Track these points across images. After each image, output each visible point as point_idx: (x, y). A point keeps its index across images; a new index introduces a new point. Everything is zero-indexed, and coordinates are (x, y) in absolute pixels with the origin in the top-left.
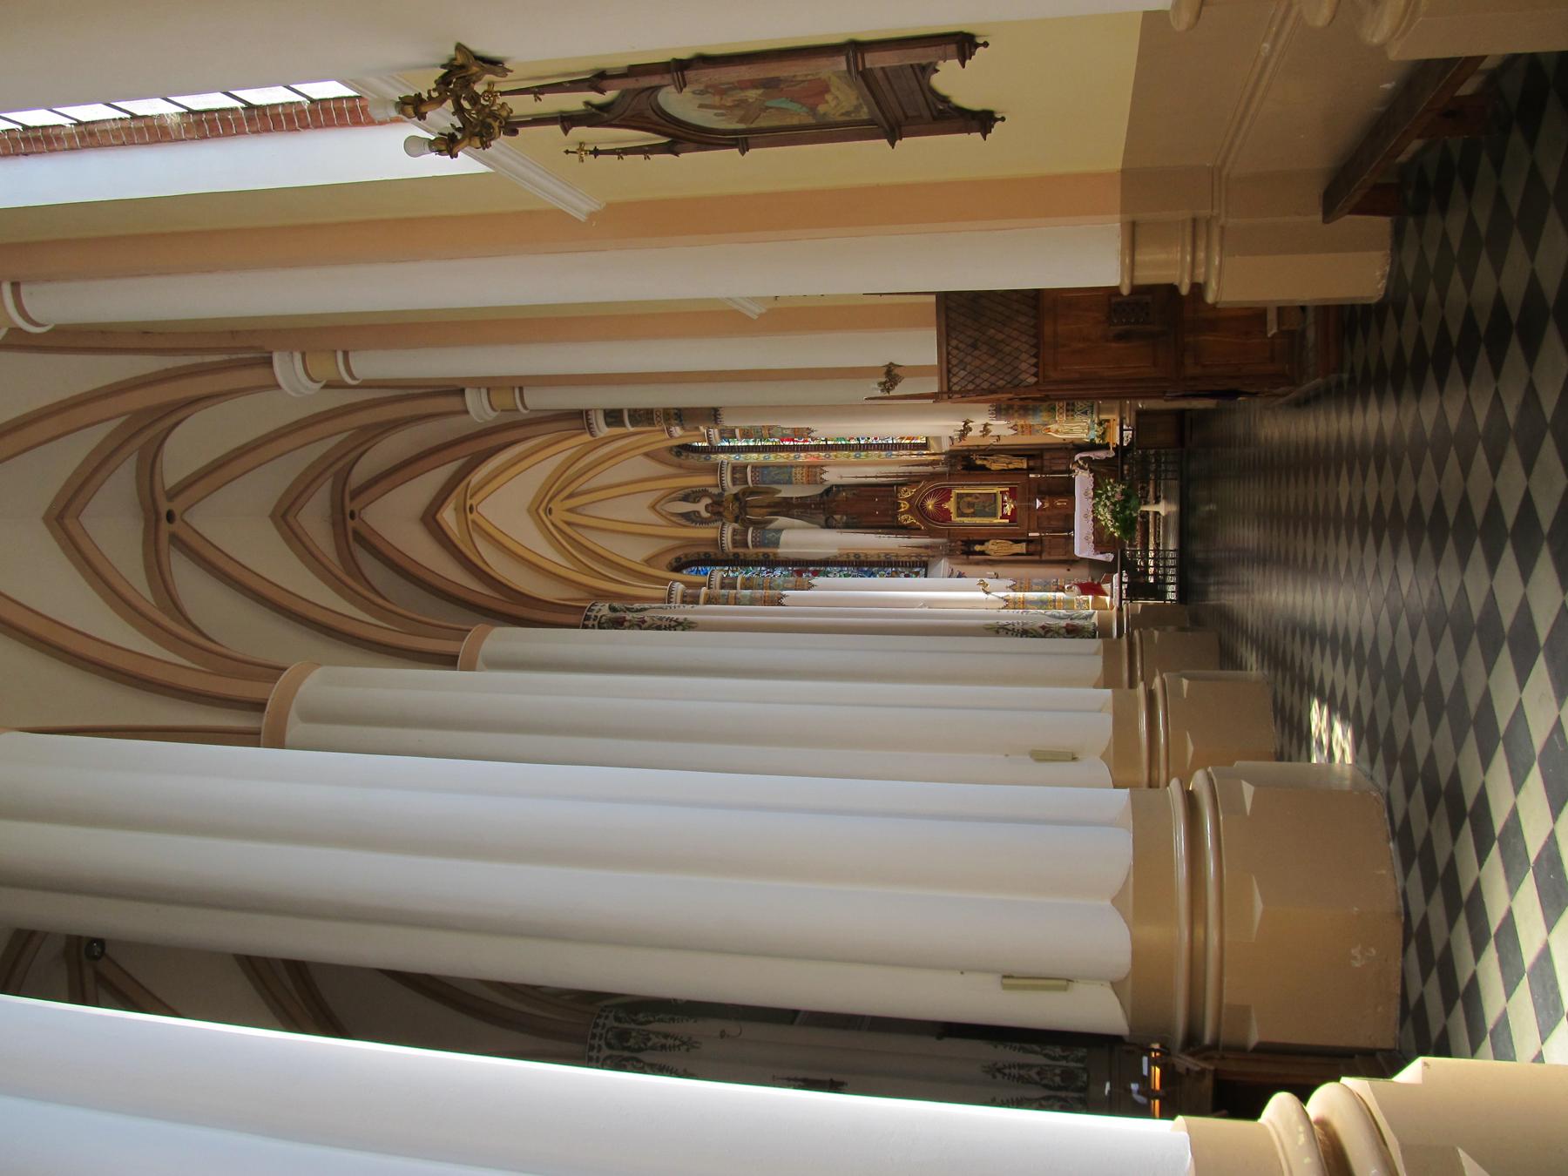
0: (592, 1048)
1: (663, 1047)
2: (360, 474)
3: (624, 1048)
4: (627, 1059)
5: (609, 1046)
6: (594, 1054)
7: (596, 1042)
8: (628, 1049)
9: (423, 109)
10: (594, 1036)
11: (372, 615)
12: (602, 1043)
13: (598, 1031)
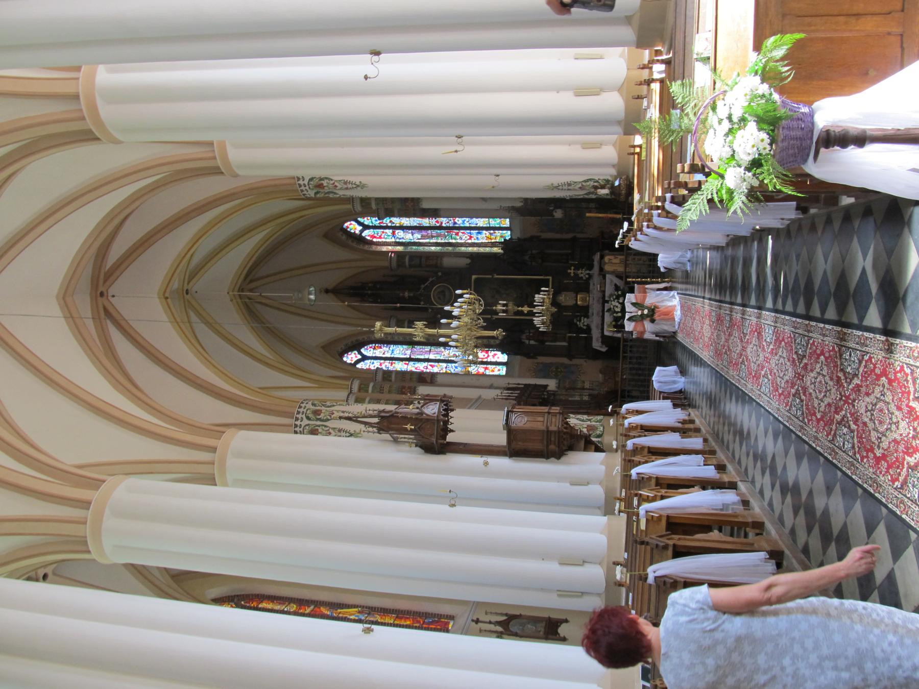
0: (297, 419)
5: (308, 418)
7: (299, 416)
10: (298, 413)
11: (166, 422)
12: (304, 416)
13: (301, 410)
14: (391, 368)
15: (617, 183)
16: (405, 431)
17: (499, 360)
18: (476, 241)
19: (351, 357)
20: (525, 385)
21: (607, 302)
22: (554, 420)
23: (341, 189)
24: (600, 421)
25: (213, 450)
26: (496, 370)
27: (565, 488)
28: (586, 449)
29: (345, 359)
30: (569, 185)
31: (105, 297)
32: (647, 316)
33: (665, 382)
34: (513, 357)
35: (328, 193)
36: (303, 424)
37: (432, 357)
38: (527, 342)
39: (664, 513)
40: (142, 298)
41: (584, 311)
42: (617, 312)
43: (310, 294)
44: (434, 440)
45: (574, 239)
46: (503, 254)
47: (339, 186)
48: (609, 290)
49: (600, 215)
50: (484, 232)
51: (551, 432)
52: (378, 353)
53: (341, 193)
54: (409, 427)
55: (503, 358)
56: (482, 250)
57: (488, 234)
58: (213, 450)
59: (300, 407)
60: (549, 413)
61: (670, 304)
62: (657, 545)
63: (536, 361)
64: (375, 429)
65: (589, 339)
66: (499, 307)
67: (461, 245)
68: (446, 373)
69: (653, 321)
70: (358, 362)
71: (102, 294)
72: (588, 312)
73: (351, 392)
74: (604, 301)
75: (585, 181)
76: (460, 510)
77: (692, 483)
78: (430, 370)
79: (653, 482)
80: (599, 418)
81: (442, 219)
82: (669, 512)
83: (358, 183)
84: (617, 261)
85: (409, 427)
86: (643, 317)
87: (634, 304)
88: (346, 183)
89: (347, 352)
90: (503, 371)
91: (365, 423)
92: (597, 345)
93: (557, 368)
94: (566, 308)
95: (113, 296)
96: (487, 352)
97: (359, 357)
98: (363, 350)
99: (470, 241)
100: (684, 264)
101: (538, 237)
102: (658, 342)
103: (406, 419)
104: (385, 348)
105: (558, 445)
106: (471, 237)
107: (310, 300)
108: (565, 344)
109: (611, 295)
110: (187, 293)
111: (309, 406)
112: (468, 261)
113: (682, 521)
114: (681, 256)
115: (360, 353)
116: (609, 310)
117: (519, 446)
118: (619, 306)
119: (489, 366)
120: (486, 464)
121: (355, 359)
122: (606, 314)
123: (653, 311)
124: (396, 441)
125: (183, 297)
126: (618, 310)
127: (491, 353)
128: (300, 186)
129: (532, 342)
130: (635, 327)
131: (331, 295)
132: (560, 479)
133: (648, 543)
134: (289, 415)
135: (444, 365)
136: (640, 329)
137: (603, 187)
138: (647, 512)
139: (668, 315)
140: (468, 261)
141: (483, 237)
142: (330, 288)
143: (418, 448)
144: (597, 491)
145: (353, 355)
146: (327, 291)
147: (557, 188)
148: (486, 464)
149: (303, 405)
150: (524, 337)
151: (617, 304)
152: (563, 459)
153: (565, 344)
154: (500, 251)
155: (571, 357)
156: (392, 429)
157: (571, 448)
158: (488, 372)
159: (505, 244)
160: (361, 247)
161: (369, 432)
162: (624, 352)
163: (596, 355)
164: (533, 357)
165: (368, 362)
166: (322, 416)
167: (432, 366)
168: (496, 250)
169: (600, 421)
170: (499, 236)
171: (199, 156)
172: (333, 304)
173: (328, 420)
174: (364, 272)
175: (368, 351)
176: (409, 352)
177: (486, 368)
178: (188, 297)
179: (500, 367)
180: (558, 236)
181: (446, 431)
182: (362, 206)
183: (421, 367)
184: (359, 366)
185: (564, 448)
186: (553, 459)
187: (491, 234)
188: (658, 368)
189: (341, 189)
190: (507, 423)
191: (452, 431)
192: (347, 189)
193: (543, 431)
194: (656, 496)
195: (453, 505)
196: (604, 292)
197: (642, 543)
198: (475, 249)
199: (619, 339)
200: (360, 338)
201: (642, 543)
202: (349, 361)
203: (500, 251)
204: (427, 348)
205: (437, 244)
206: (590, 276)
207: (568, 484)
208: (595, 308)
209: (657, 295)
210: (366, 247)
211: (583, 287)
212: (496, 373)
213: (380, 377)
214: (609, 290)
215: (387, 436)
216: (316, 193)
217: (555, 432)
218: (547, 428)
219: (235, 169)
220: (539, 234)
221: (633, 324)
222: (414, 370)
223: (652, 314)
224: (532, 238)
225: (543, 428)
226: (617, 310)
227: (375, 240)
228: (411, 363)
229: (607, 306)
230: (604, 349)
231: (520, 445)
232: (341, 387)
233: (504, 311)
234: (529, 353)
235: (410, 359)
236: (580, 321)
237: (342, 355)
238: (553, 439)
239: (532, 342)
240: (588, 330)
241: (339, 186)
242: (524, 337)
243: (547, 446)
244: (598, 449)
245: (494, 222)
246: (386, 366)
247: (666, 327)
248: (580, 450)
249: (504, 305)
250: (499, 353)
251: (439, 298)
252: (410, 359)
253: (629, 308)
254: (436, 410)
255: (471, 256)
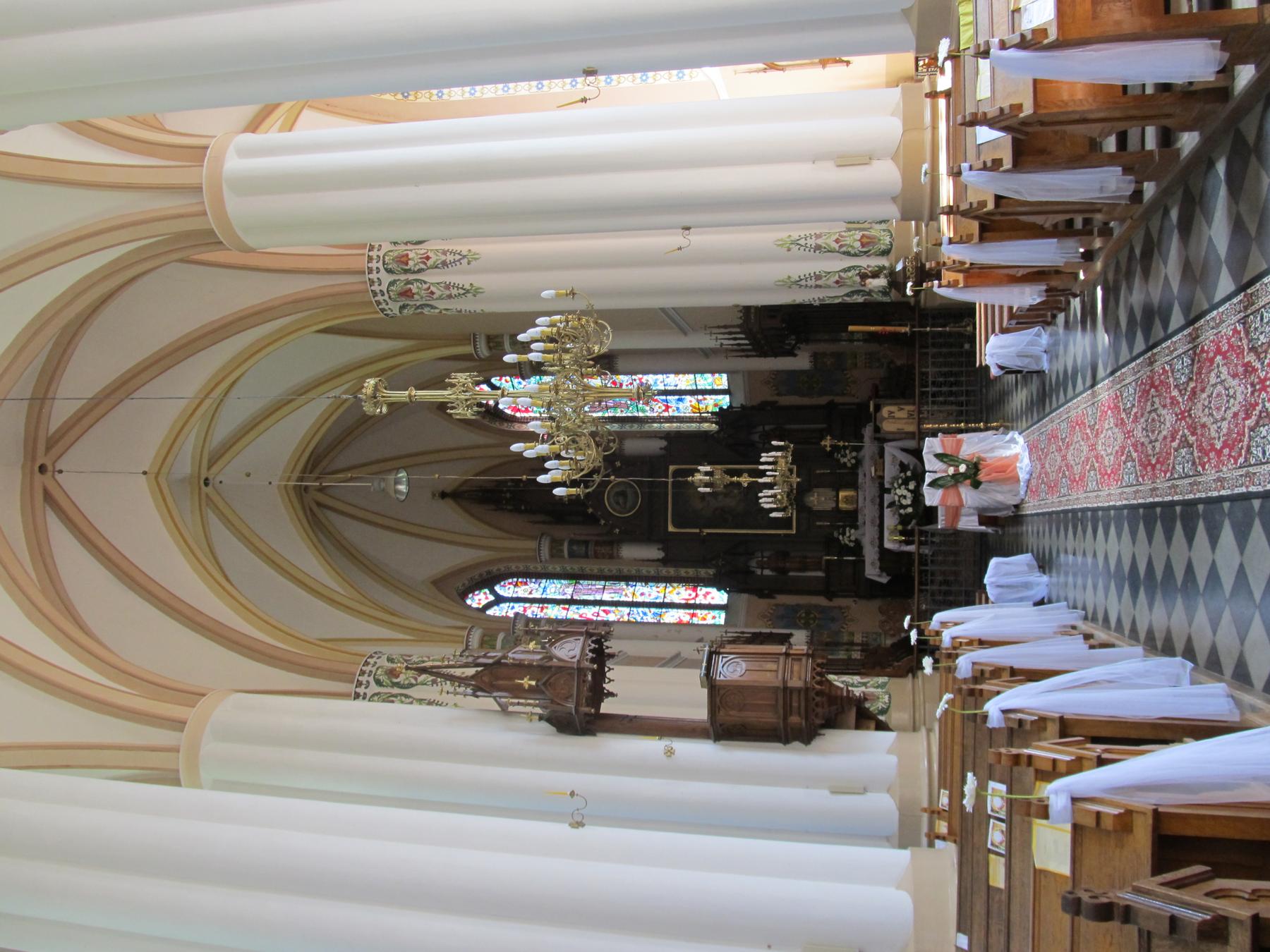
0: (359, 684)
1: (444, 264)
2: (61, 412)
3: (406, 271)
4: (395, 696)
5: (379, 683)
6: (361, 690)
7: (364, 679)
8: (398, 685)
9: (876, 537)
10: (362, 673)
11: (109, 678)
12: (371, 679)
13: (367, 669)
14: (541, 615)
15: (899, 267)
16: (518, 692)
17: (713, 602)
18: (676, 414)
19: (479, 599)
20: (754, 634)
21: (888, 491)
22: (796, 668)
23: (440, 298)
24: (882, 686)
25: (179, 725)
26: (709, 617)
27: (820, 798)
28: (858, 726)
29: (469, 602)
30: (818, 277)
31: (49, 474)
32: (965, 476)
33: (1008, 586)
34: (736, 596)
35: (422, 306)
36: (369, 692)
37: (607, 597)
38: (759, 572)
39: (1145, 802)
40: (117, 487)
41: (851, 518)
42: (905, 507)
43: (397, 482)
44: (571, 705)
45: (831, 404)
46: (718, 432)
47: (438, 293)
48: (890, 471)
49: (872, 328)
50: (688, 398)
51: (792, 690)
52: (522, 592)
53: (442, 305)
54: (527, 682)
55: (720, 597)
56: (685, 427)
57: (694, 403)
58: (179, 725)
59: (366, 663)
60: (787, 655)
61: (1008, 453)
62: (1174, 923)
63: (772, 601)
64: (469, 691)
65: (860, 563)
66: (698, 477)
67: (653, 420)
68: (629, 622)
69: (976, 485)
70: (489, 606)
71: (42, 469)
72: (856, 519)
73: (467, 648)
74: (883, 491)
75: (845, 270)
76: (591, 833)
77: (1167, 736)
78: (603, 617)
79: (1053, 728)
80: (881, 680)
81: (622, 377)
82: (1169, 801)
83: (467, 287)
84: (903, 414)
85: (527, 682)
86: (957, 478)
87: (938, 456)
88: (448, 287)
89: (473, 592)
90: (720, 618)
91: (452, 678)
92: (872, 571)
93: (808, 613)
94: (821, 515)
95: (61, 472)
96: (695, 590)
97: (492, 598)
98: (497, 588)
99: (666, 414)
100: (1037, 359)
101: (773, 404)
102: (983, 535)
103: (522, 668)
104: (532, 585)
105: (805, 715)
106: (667, 408)
107: (397, 491)
108: (820, 574)
109: (895, 479)
110: (206, 484)
111: (383, 662)
112: (663, 443)
113: (1208, 832)
114: (1031, 343)
115: (493, 592)
116: (892, 504)
117: (732, 719)
118: (909, 495)
119: (698, 612)
120: (670, 752)
121: (484, 602)
122: (887, 512)
123: (975, 467)
124: (504, 710)
125: (198, 490)
126: (908, 502)
127: (702, 590)
128: (375, 294)
129: (767, 572)
130: (943, 498)
131: (449, 501)
132: (810, 781)
133: (1127, 914)
134: (345, 677)
135: (626, 610)
136: (952, 501)
137: (875, 275)
138: (1074, 800)
139: (1006, 473)
140: (663, 443)
141: (686, 407)
142: (448, 490)
143: (544, 725)
144: (883, 804)
145: (482, 596)
146: (443, 495)
147: (798, 283)
148: (670, 752)
149: (371, 661)
150: (753, 563)
151: (905, 492)
152: (817, 742)
153: (820, 574)
154: (714, 427)
155: (830, 595)
156: (499, 689)
157: (833, 723)
158: (695, 621)
159: (721, 415)
160: (497, 425)
161: (456, 694)
162: (921, 583)
163: (871, 590)
164: (770, 596)
165: (504, 606)
166: (401, 679)
167: (606, 612)
168: (706, 426)
169: (882, 686)
170: (711, 404)
171: (182, 211)
172: (452, 516)
173: (411, 685)
174: (505, 463)
175: (505, 590)
176: (570, 590)
177: (693, 615)
178: (209, 490)
179: (716, 613)
180: (806, 401)
181: (598, 694)
182: (490, 348)
183: (589, 612)
184: (490, 612)
185: (818, 722)
186: (797, 744)
187: (699, 401)
188: (994, 562)
189: (440, 298)
190: (708, 674)
191: (611, 694)
192: (450, 297)
193: (778, 688)
194: (1080, 759)
195: (580, 824)
196: (882, 477)
197: (1105, 912)
198: (675, 426)
199: (909, 554)
200: (494, 569)
201: (1105, 912)
202: (475, 605)
203: (714, 427)
204: (600, 584)
205: (614, 420)
206: (859, 462)
207: (826, 792)
208: (868, 513)
209: (981, 441)
210: (505, 426)
211: (849, 479)
212: (710, 621)
213: (520, 626)
214: (890, 471)
215: (488, 702)
216: (402, 307)
217: (799, 690)
218: (785, 682)
219: (240, 234)
220: (776, 398)
221: (940, 492)
222: (577, 617)
223: (973, 474)
224: (763, 406)
225: (777, 682)
226: (904, 502)
227: (518, 415)
228: (573, 608)
229: (887, 498)
230: (884, 580)
231: (731, 716)
232: (452, 640)
233: (706, 485)
234: (762, 590)
235: (572, 602)
236: (844, 534)
237: (464, 595)
238: (795, 704)
239: (767, 572)
240: (858, 548)
241: (438, 293)
242: (753, 563)
243: (785, 718)
244: (882, 726)
245: (705, 381)
246: (533, 611)
247: (997, 496)
248: (848, 728)
249: (707, 474)
250: (713, 591)
251: (618, 503)
252: (572, 602)
253: (931, 463)
254: (577, 652)
255: (668, 436)
